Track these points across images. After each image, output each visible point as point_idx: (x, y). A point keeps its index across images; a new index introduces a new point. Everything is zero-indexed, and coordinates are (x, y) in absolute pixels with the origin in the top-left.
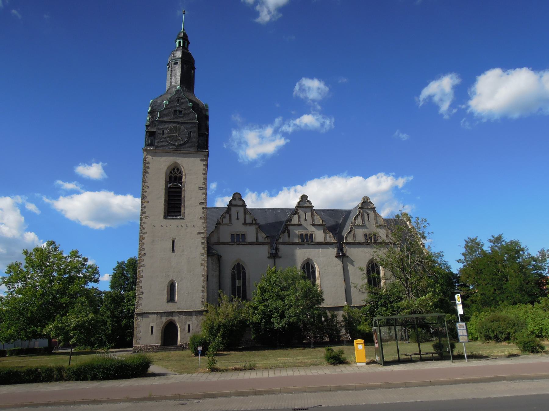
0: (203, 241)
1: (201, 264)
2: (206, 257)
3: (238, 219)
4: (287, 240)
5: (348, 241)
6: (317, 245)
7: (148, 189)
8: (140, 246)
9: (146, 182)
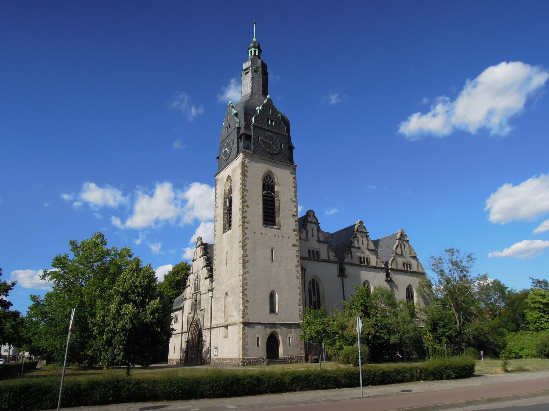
0: (297, 254)
1: (297, 276)
2: (300, 270)
4: (350, 261)
5: (392, 268)
6: (372, 269)
7: (247, 193)
8: (243, 252)
9: (245, 186)
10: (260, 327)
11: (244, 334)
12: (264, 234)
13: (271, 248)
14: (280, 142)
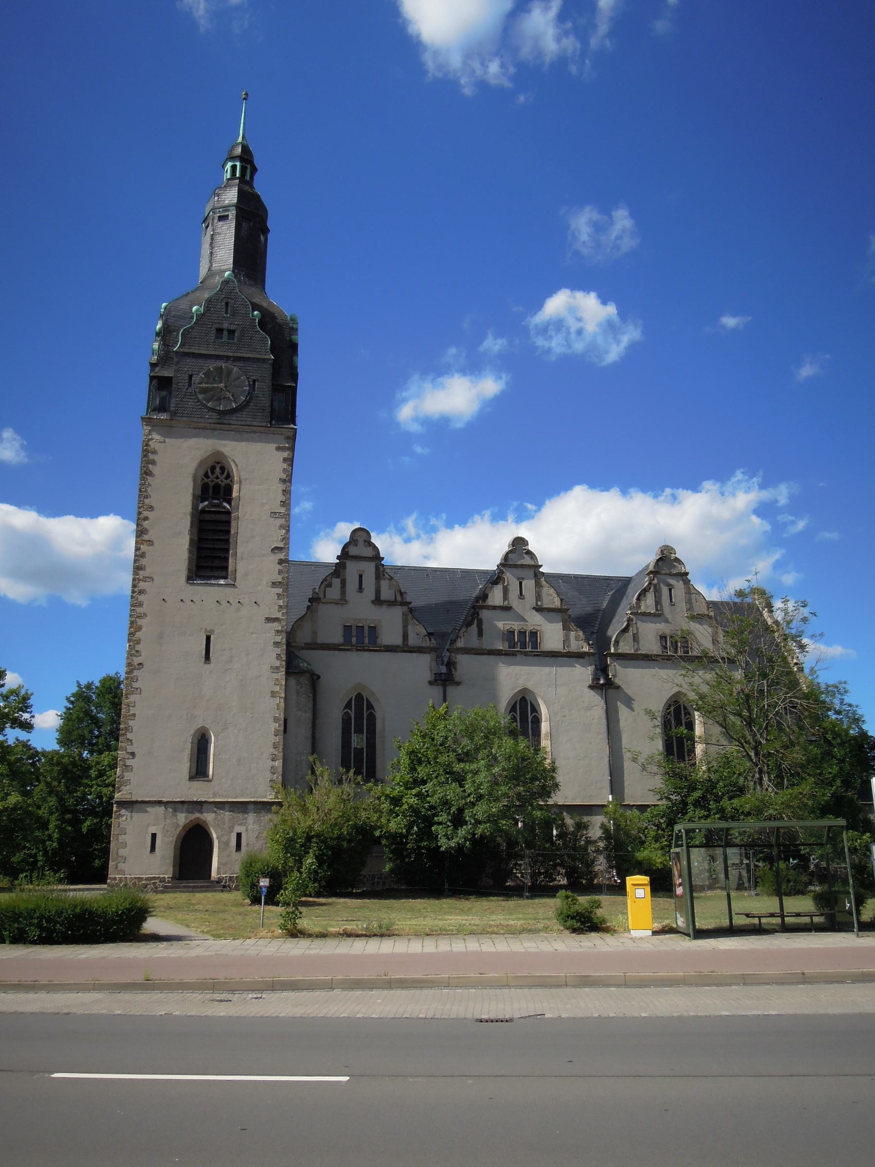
0: (278, 639)
2: (284, 677)
3: (360, 589)
4: (474, 643)
5: (620, 651)
8: (130, 646)
9: (146, 497)
10: (161, 809)
11: (119, 827)
12: (188, 602)
13: (205, 632)
14: (248, 379)
